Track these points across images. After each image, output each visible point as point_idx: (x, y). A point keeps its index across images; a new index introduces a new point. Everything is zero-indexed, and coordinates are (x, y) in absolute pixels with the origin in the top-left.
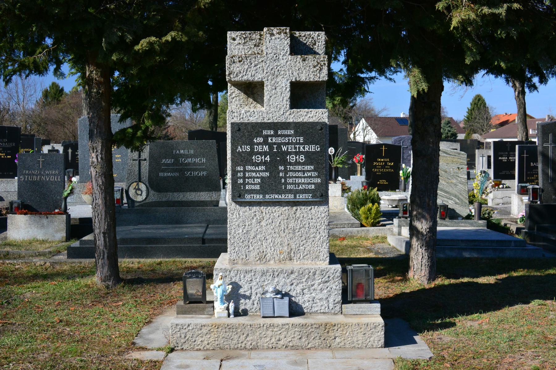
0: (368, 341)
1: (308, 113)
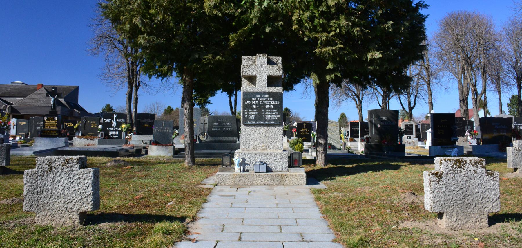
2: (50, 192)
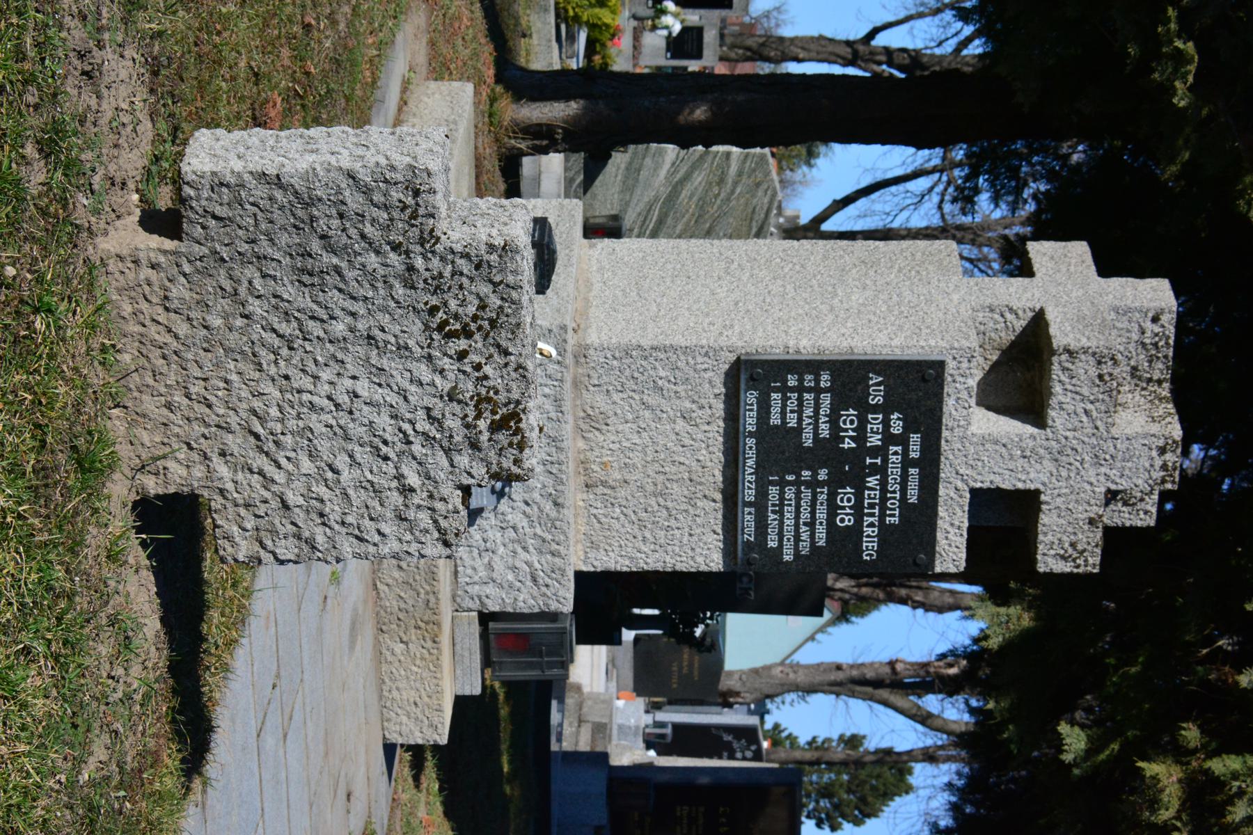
0: (399, 711)
1: (959, 528)
2: (315, 329)
